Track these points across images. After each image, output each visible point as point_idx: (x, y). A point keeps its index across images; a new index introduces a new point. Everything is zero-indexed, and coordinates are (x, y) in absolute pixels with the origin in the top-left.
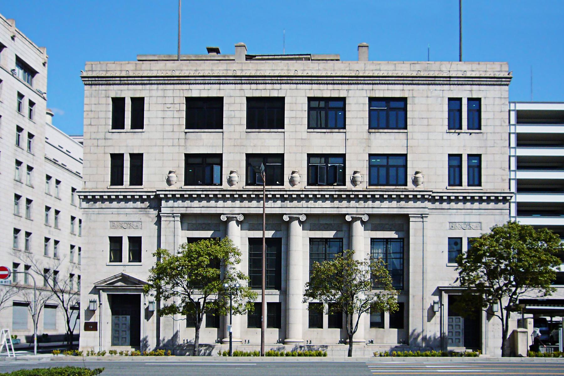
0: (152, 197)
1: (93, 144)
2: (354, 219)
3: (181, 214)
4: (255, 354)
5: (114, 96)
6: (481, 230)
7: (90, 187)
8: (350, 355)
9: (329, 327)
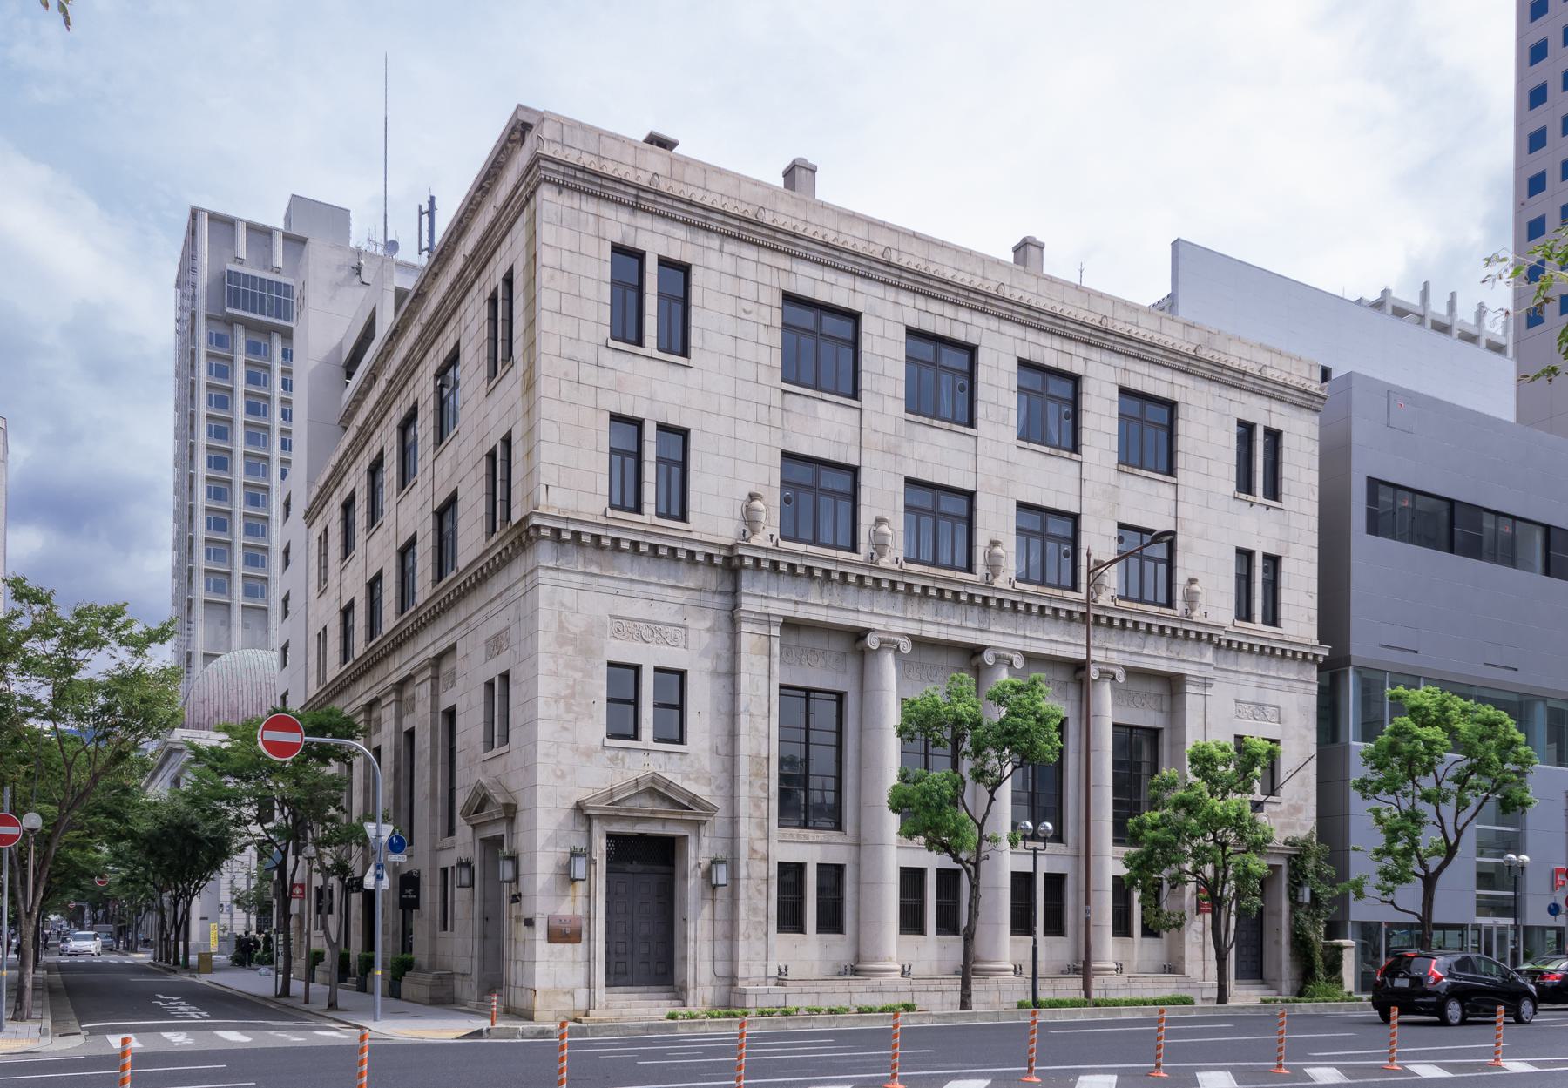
0: (717, 560)
1: (566, 374)
2: (884, 644)
3: (785, 618)
4: (1074, 1004)
5: (618, 240)
6: (1279, 723)
7: (559, 504)
8: (965, 1003)
9: (938, 933)
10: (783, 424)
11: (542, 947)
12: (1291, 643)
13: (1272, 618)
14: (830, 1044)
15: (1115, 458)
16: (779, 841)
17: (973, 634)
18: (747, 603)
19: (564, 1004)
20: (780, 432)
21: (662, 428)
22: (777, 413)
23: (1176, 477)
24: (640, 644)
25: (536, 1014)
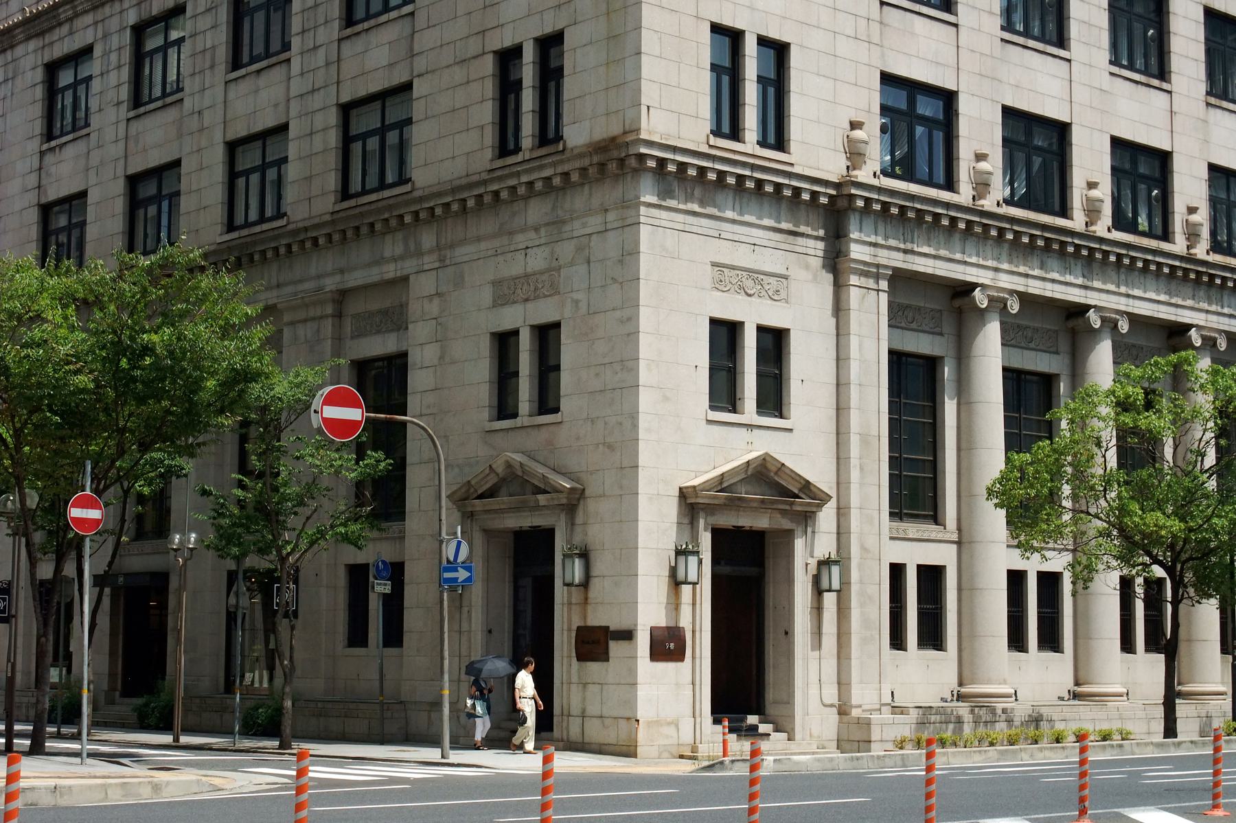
10: (881, 40)
11: (646, 667)
12: (675, 149)
13: (775, 134)
14: (1047, 777)
15: (1202, 87)
16: (892, 538)
17: (1076, 291)
18: (858, 252)
19: (667, 737)
20: (879, 48)
21: (763, 41)
22: (875, 27)
23: (1170, 83)
24: (742, 297)
25: (639, 750)
